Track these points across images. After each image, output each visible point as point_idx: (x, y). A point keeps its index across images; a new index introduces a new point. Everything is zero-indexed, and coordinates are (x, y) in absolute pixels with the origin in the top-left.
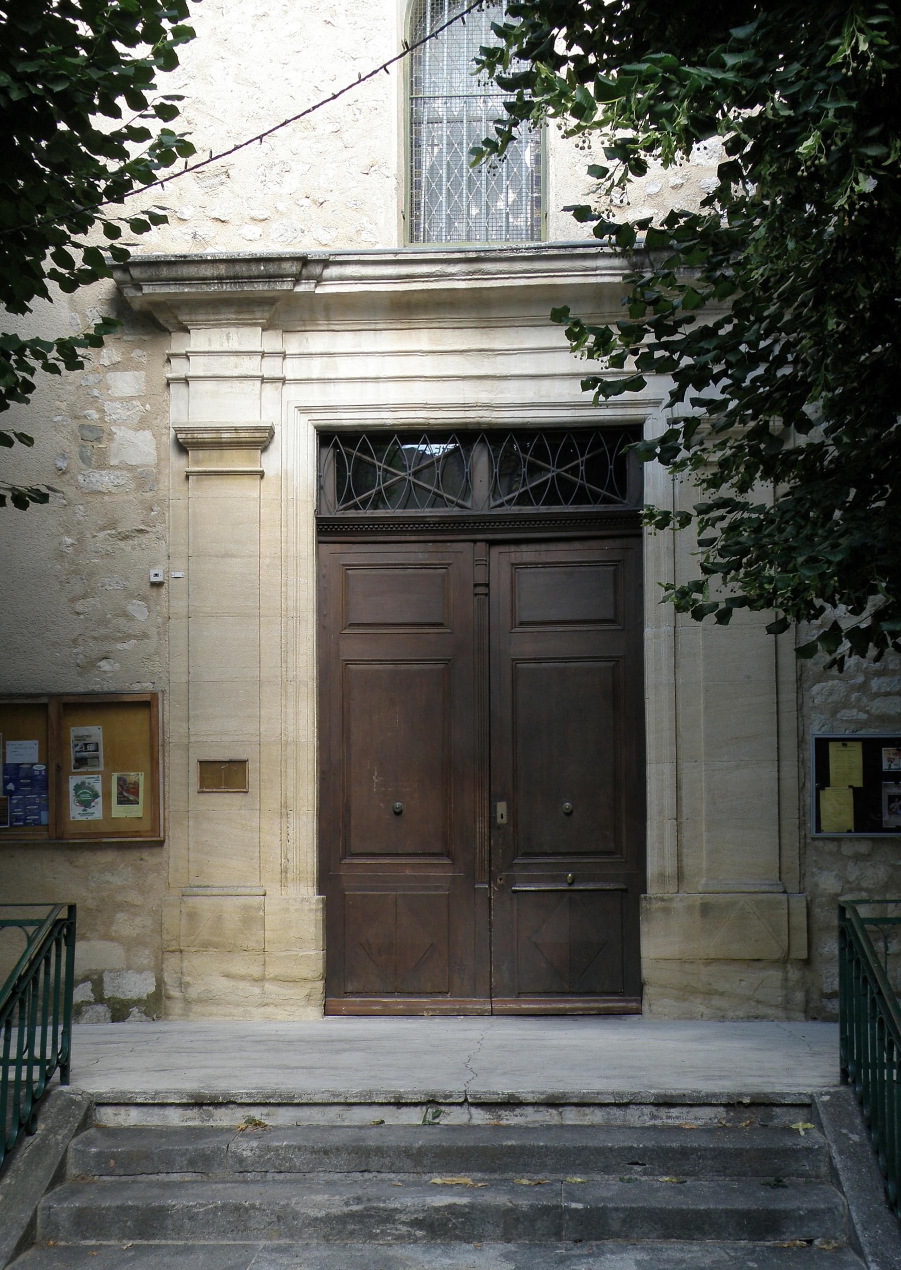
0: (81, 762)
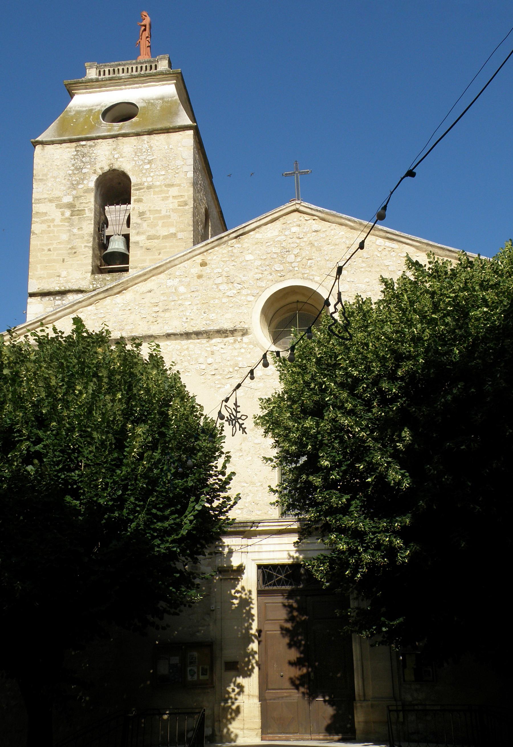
0: (191, 663)
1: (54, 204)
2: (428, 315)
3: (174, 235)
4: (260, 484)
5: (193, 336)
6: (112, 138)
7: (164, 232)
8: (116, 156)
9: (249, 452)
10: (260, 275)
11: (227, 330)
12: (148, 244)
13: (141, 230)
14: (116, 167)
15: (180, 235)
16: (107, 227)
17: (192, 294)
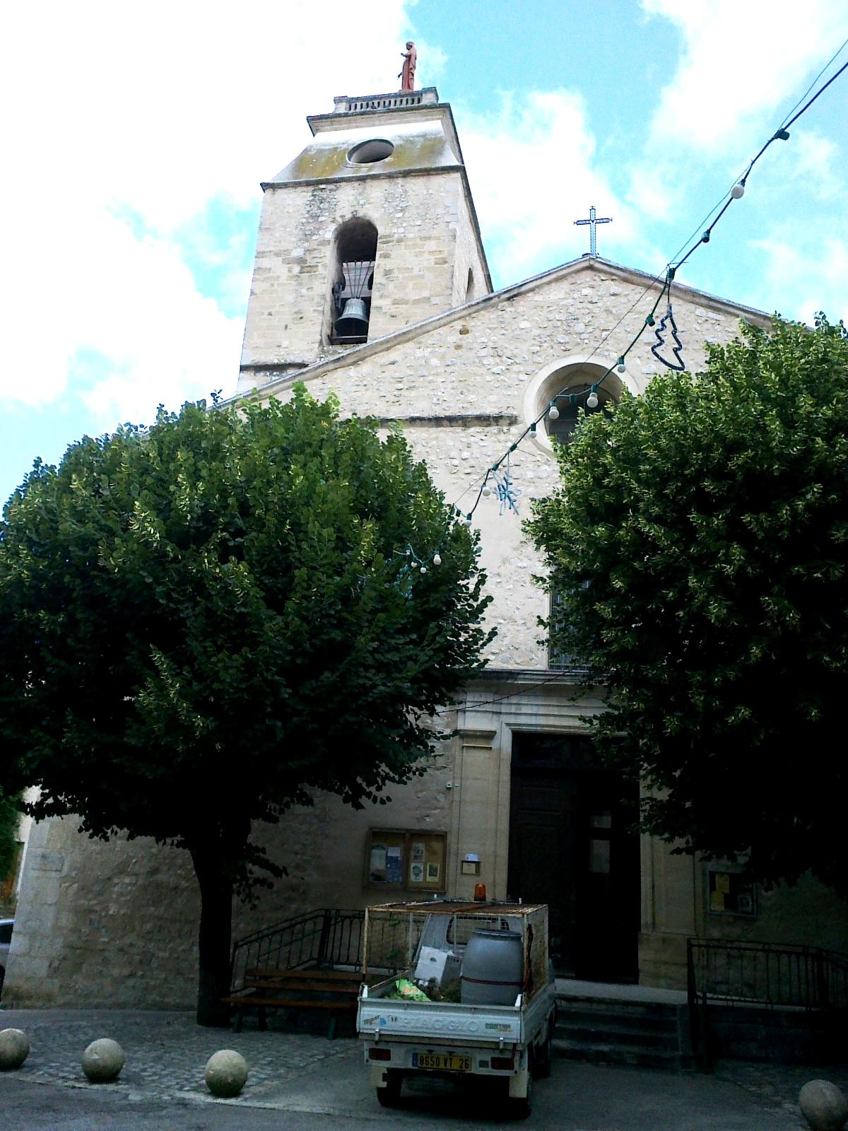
0: (416, 857)
1: (281, 259)
2: (773, 393)
3: (427, 300)
4: (523, 621)
5: (445, 422)
6: (358, 180)
7: (414, 296)
8: (362, 202)
9: (510, 578)
10: (538, 348)
11: (489, 417)
12: (393, 310)
13: (386, 293)
14: (360, 214)
15: (434, 300)
16: (343, 288)
17: (446, 369)
